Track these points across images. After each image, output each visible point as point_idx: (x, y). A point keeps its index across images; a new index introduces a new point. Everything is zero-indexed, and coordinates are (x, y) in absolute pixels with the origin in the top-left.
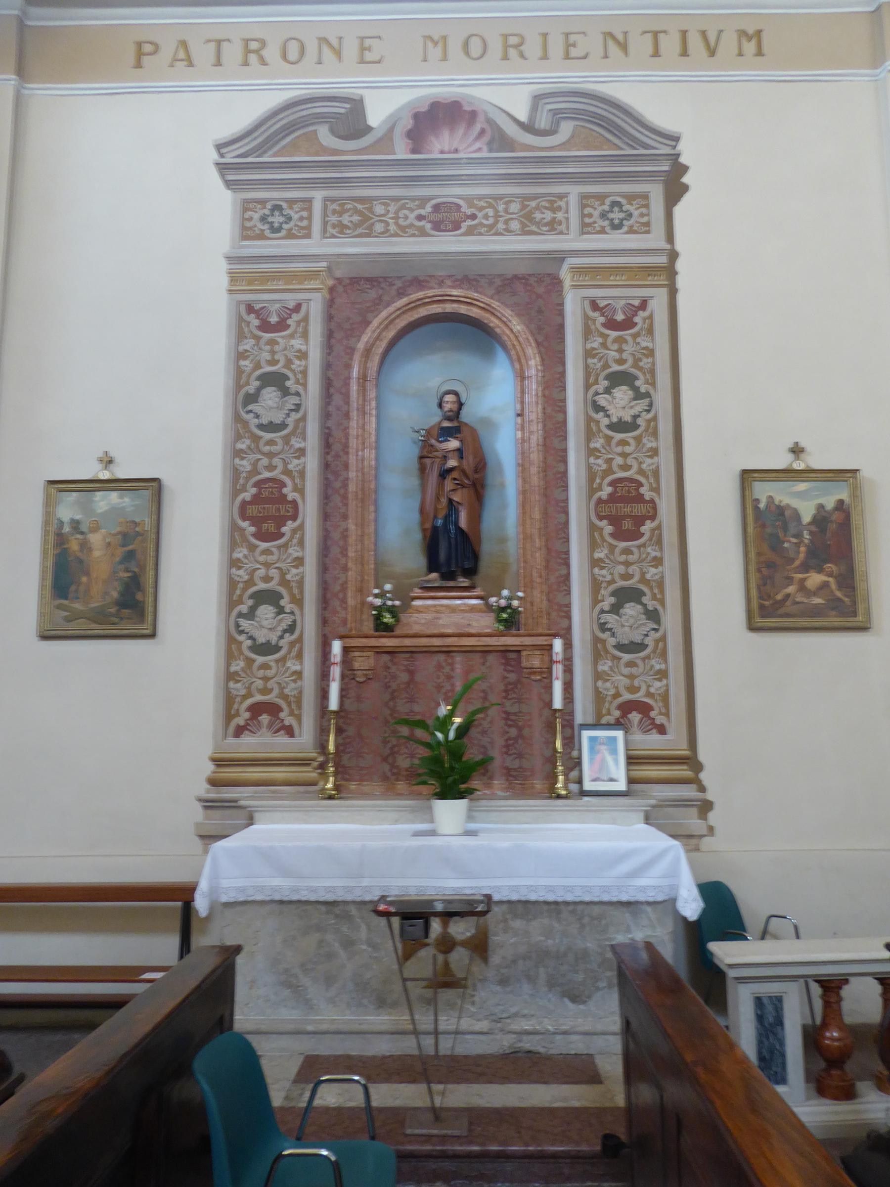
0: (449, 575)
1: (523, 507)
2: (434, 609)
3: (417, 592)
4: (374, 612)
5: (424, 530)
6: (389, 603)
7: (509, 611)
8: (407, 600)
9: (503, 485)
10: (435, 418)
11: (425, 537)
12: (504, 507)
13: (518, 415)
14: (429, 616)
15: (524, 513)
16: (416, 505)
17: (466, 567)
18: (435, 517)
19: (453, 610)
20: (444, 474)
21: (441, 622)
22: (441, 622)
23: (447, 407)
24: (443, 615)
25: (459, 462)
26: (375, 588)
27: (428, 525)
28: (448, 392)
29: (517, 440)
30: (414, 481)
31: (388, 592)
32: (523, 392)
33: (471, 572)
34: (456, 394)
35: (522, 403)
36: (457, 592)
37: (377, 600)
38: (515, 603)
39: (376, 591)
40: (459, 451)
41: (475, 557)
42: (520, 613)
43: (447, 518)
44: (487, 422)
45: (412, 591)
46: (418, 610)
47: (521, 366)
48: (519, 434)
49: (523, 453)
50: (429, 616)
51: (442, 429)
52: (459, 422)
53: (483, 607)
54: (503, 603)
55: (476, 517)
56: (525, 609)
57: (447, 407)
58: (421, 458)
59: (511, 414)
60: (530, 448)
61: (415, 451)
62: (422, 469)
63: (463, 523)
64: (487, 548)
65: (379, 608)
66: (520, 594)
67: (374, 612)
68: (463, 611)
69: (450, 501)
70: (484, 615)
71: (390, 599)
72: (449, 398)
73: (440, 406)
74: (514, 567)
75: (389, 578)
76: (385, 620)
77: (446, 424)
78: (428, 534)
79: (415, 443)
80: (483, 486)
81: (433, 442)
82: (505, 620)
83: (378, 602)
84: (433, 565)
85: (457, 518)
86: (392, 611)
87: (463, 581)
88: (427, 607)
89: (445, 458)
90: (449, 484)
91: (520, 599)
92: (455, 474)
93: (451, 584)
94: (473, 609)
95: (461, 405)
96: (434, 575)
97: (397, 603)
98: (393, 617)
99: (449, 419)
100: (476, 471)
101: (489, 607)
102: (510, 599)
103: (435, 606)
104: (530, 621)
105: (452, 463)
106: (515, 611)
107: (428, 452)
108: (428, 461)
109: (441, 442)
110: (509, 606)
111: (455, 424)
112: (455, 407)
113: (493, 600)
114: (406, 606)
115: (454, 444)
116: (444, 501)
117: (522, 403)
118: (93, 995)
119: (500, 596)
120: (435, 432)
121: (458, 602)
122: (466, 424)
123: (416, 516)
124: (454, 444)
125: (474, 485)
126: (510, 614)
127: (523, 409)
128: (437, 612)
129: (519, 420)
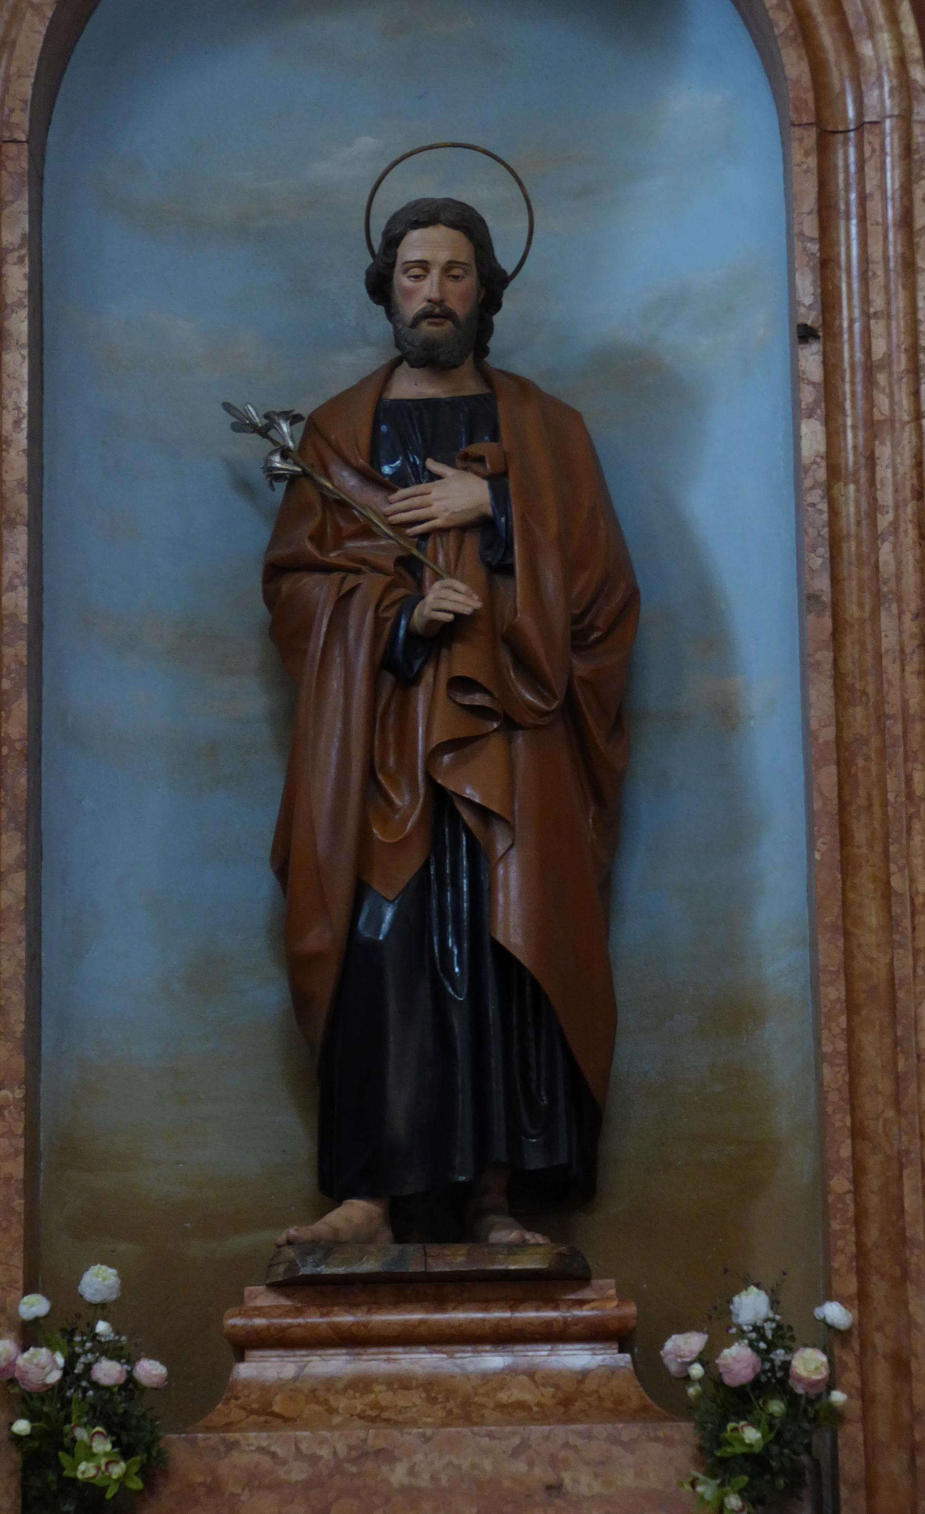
0: (432, 1212)
1: (845, 839)
2: (359, 1404)
3: (263, 1307)
4: (22, 1426)
5: (297, 967)
6: (108, 1371)
7: (776, 1407)
8: (206, 1363)
9: (727, 717)
10: (352, 352)
11: (301, 1001)
12: (735, 832)
13: (805, 334)
14: (329, 1444)
15: (847, 866)
16: (255, 823)
17: (535, 1161)
18: (360, 890)
19: (461, 1405)
20: (405, 657)
21: (398, 1475)
22: (398, 1475)
23: (417, 294)
24: (411, 1436)
25: (490, 597)
26: (28, 1290)
27: (320, 938)
28: (423, 215)
29: (799, 469)
30: (246, 700)
31: (101, 1309)
32: (827, 210)
33: (561, 1192)
34: (468, 223)
35: (826, 265)
36: (486, 1303)
37: (41, 1355)
38: (809, 1363)
39: (34, 1306)
40: (488, 536)
41: (586, 1109)
42: (836, 1416)
43: (419, 897)
44: (644, 378)
45: (238, 1300)
46: (267, 1410)
47: (818, 68)
48: (813, 436)
49: (843, 752)
50: (329, 1444)
51: (389, 412)
52: (485, 375)
53: (635, 1394)
54: (738, 1360)
55: (583, 888)
56: (865, 1395)
57: (417, 294)
58: (276, 571)
59: (764, 325)
60: (874, 508)
61: (247, 537)
62: (286, 635)
63: (511, 926)
64: (644, 1059)
65: (53, 1408)
66: (834, 1313)
67: (22, 1426)
68: (517, 1411)
69: (441, 802)
70: (628, 1431)
71: (113, 1352)
72: (418, 245)
73: (380, 286)
74: (799, 1162)
75: (101, 1229)
76: (85, 1470)
77: (410, 386)
78: (324, 985)
79: (244, 486)
80: (620, 720)
81: (347, 482)
82: (756, 1462)
83: (44, 1365)
84: (345, 1158)
85: (481, 896)
86: (127, 1418)
87: (516, 1246)
88: (322, 1393)
89: (411, 571)
90: (431, 714)
91: (830, 1339)
92: (464, 660)
93: (453, 1259)
94: (571, 1399)
95: (492, 284)
96: (355, 1213)
97: (150, 1370)
98: (125, 1451)
99: (429, 359)
100: (579, 640)
101: (660, 1388)
102: (774, 1340)
103: (361, 1384)
104: (894, 1465)
105: (449, 596)
106: (808, 1409)
107: (318, 538)
108: (319, 591)
109: (388, 486)
110: (774, 1380)
111: (471, 387)
112: (460, 295)
113: (683, 1346)
114: (202, 1385)
115: (457, 493)
116: (408, 803)
117: (826, 265)
118: (280, 816)
119: (720, 1327)
120: (356, 431)
121: (494, 1361)
122: (524, 386)
123: (253, 887)
124: (457, 493)
125: (570, 708)
126: (777, 1434)
127: (828, 301)
128: (375, 1417)
129: (811, 359)
